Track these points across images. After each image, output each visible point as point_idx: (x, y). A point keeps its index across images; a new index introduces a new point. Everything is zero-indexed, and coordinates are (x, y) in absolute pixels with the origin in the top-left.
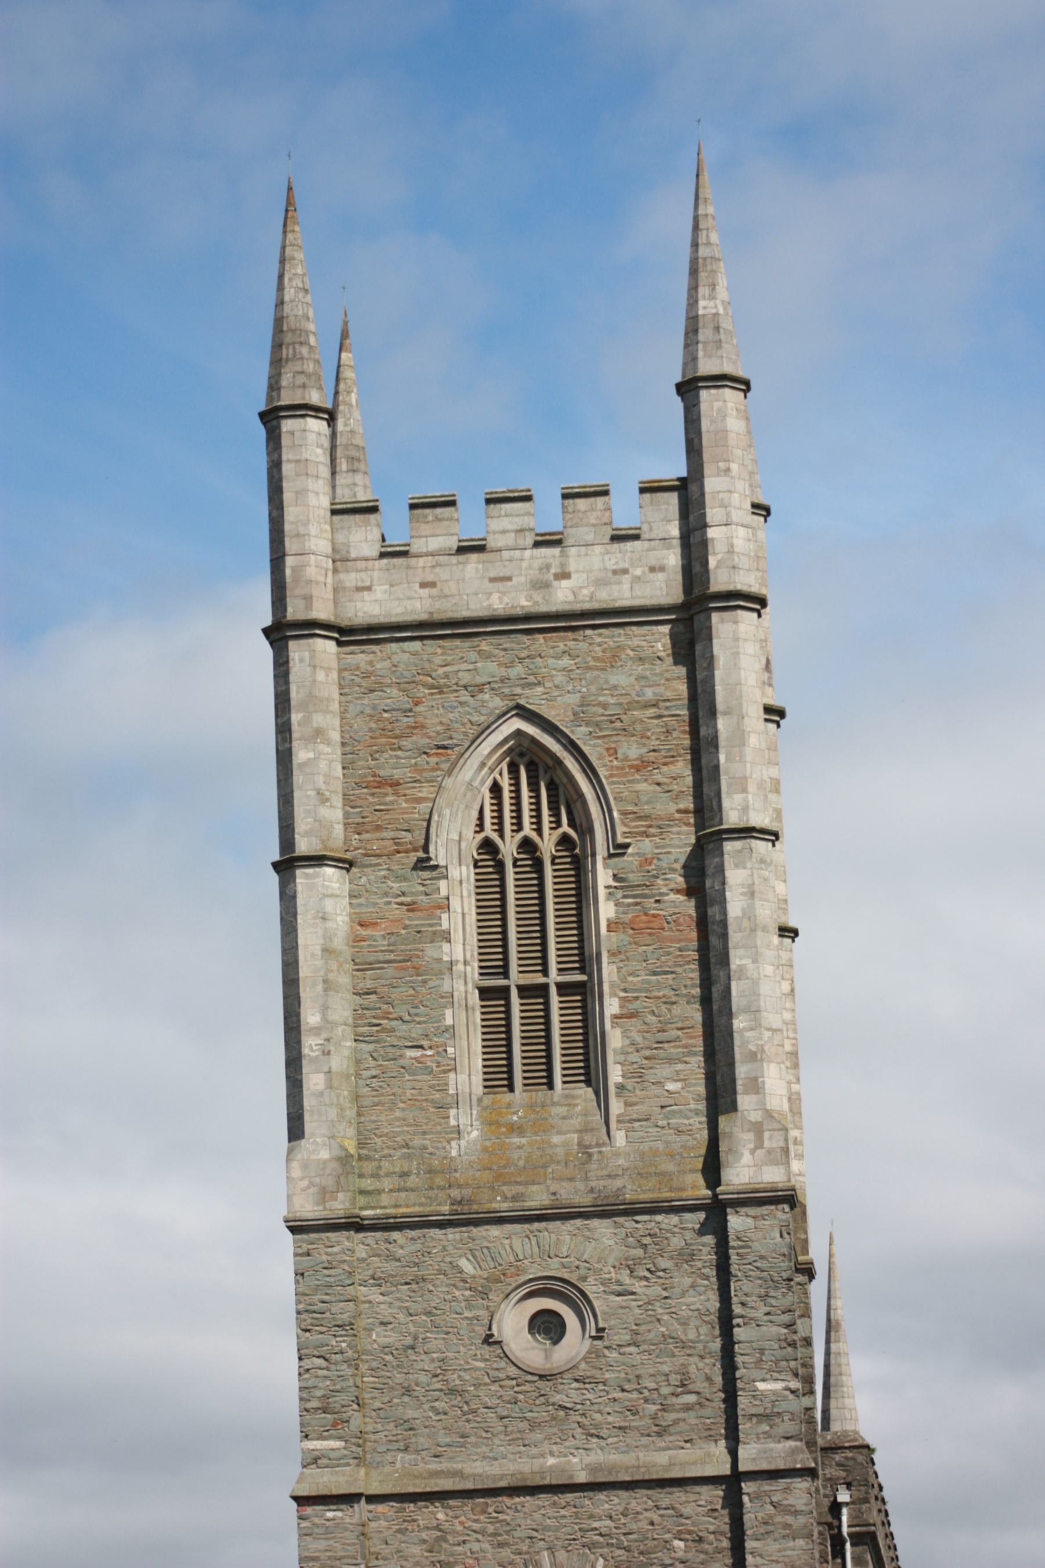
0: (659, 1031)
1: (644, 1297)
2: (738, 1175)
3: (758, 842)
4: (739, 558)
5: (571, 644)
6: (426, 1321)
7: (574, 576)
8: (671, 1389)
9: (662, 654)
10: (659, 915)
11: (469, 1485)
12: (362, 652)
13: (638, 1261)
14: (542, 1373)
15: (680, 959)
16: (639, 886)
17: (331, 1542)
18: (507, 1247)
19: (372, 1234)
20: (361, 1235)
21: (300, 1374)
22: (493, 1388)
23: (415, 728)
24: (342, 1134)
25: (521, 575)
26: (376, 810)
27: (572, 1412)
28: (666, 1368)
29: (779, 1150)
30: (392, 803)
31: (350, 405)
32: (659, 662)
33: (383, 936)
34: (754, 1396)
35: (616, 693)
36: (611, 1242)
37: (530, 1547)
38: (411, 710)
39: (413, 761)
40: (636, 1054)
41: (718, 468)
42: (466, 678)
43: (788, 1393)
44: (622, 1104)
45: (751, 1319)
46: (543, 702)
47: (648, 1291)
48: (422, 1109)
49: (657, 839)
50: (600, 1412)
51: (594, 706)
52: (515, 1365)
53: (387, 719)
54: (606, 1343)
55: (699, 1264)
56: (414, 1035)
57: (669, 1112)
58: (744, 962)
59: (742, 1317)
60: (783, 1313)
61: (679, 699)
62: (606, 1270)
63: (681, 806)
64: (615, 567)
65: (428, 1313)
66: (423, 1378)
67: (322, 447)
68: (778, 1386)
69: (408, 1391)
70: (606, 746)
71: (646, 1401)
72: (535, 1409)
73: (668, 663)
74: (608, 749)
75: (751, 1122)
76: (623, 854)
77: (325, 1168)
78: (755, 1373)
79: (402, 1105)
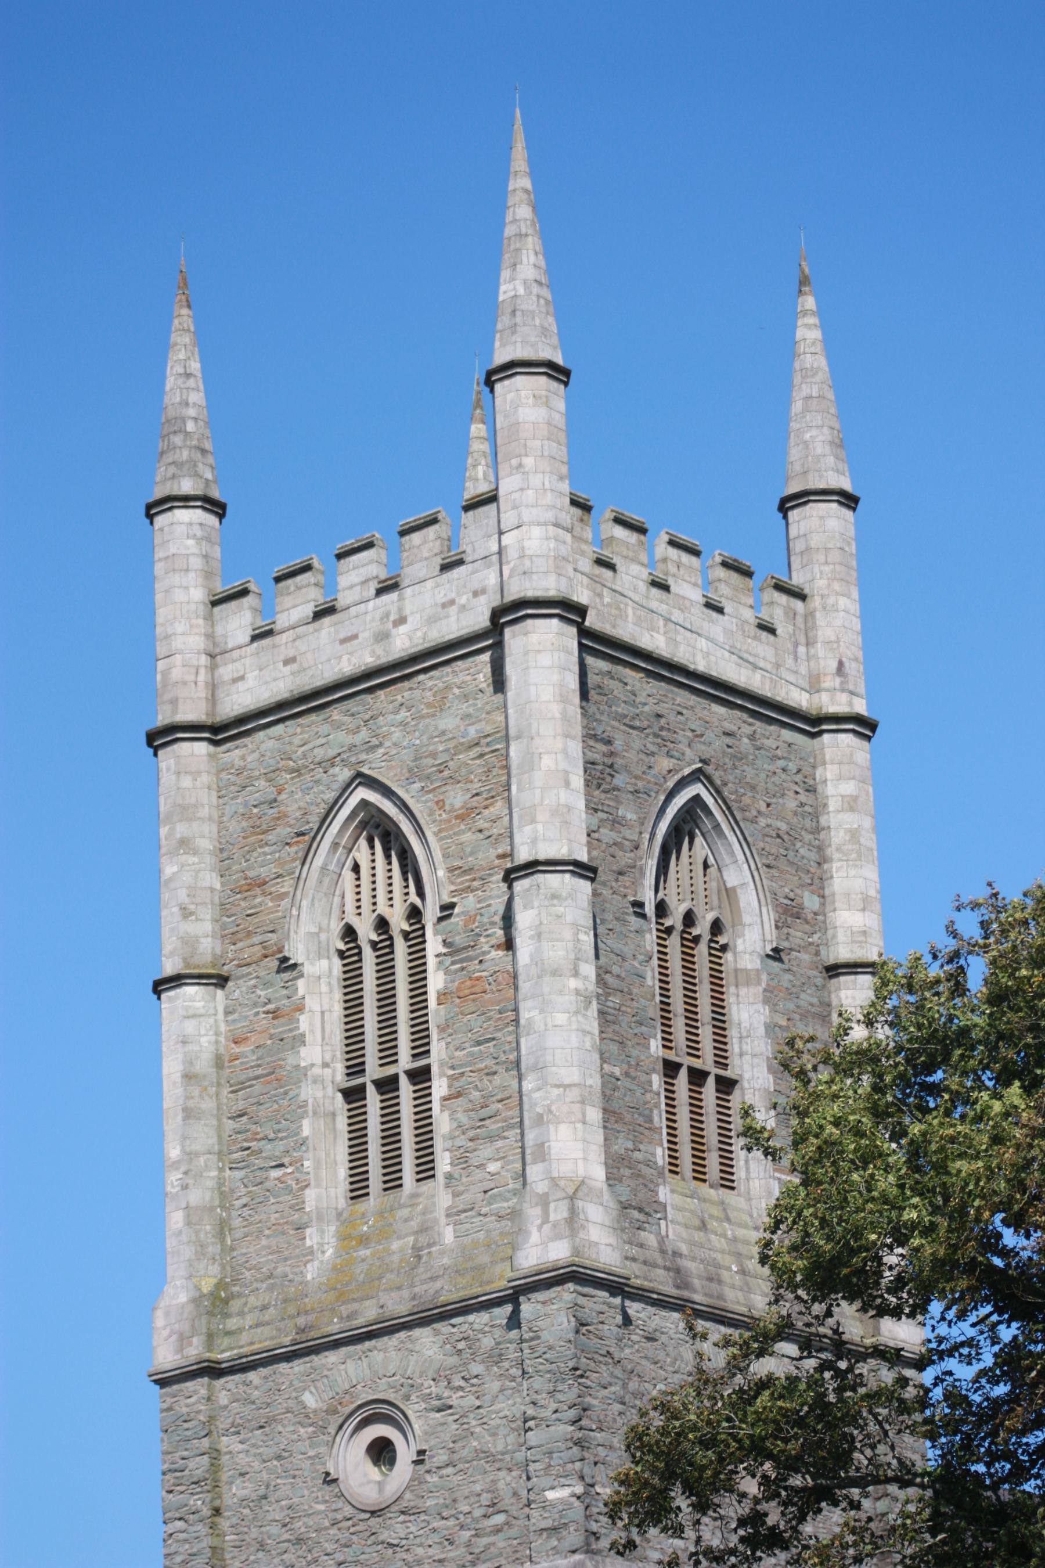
0: (482, 1107)
1: (459, 1410)
2: (527, 1257)
3: (548, 876)
4: (532, 562)
6: (276, 1466)
7: (410, 619)
9: (483, 686)
10: (481, 977)
12: (237, 748)
14: (372, 1509)
15: (500, 1023)
16: (465, 948)
18: (343, 1373)
19: (232, 1377)
20: (223, 1380)
21: (164, 1540)
22: (332, 1532)
23: (278, 819)
24: (202, 1273)
25: (365, 630)
26: (248, 916)
27: (398, 1549)
28: (478, 1488)
29: (563, 1222)
30: (260, 904)
31: (477, 480)
32: (481, 695)
33: (253, 1051)
34: (544, 1507)
35: (446, 737)
38: (275, 800)
39: (277, 855)
40: (462, 1137)
41: (511, 466)
42: (320, 754)
43: (574, 1499)
44: (450, 1196)
45: (542, 1419)
46: (383, 764)
48: (283, 1233)
49: (480, 893)
50: (421, 1545)
51: (426, 757)
52: (351, 1504)
53: (256, 815)
54: (427, 1467)
56: (277, 1154)
57: (491, 1196)
58: (532, 1014)
59: (533, 1418)
60: (570, 1408)
61: (498, 732)
62: (426, 1385)
63: (500, 851)
64: (444, 600)
65: (279, 1458)
66: (274, 1529)
69: (262, 1546)
70: (436, 799)
71: (462, 1527)
72: (367, 1550)
73: (488, 694)
74: (437, 803)
75: (538, 1194)
76: (449, 916)
77: (182, 1313)
78: (546, 1482)
79: (267, 1232)
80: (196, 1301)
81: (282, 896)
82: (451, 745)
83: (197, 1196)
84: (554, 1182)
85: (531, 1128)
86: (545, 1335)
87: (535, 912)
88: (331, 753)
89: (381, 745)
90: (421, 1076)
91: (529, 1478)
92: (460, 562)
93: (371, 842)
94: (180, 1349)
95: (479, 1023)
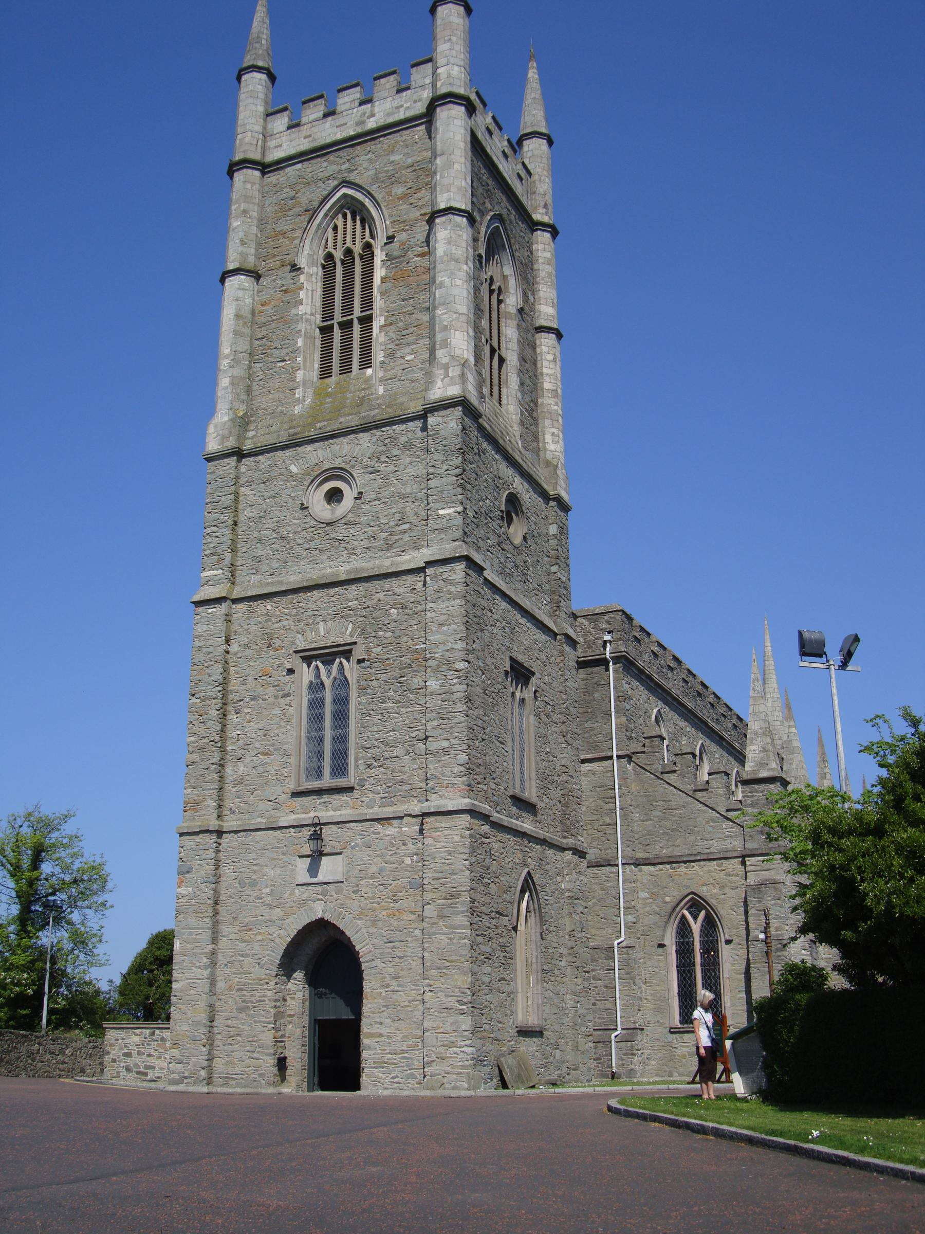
5: (373, 147)
7: (377, 115)
8: (395, 522)
11: (284, 588)
13: (381, 453)
17: (209, 626)
28: (393, 511)
36: (369, 445)
37: (314, 621)
38: (294, 197)
42: (321, 175)
47: (386, 469)
54: (362, 501)
55: (414, 450)
59: (433, 474)
62: (365, 460)
65: (273, 497)
67: (262, 85)
68: (451, 510)
76: (392, 242)
78: (438, 505)
80: (232, 420)
81: (294, 239)
82: (398, 166)
83: (237, 372)
84: (453, 357)
85: (440, 332)
86: (442, 433)
87: (448, 231)
88: (327, 175)
89: (356, 169)
90: (366, 321)
91: (428, 504)
92: (408, 88)
93: (345, 216)
94: (222, 443)
95: (405, 290)
